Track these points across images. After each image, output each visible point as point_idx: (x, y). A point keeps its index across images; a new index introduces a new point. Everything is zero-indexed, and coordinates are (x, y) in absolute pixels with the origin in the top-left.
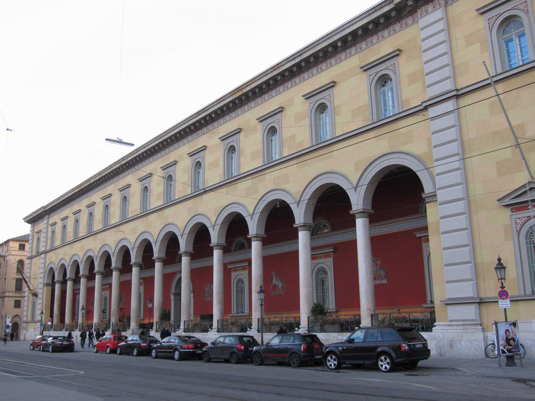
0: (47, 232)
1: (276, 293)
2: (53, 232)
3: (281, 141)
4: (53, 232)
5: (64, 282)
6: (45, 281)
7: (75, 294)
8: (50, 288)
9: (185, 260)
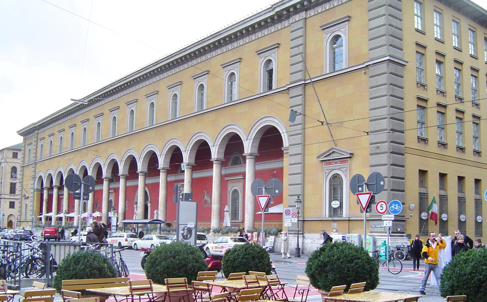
5: (51, 188)
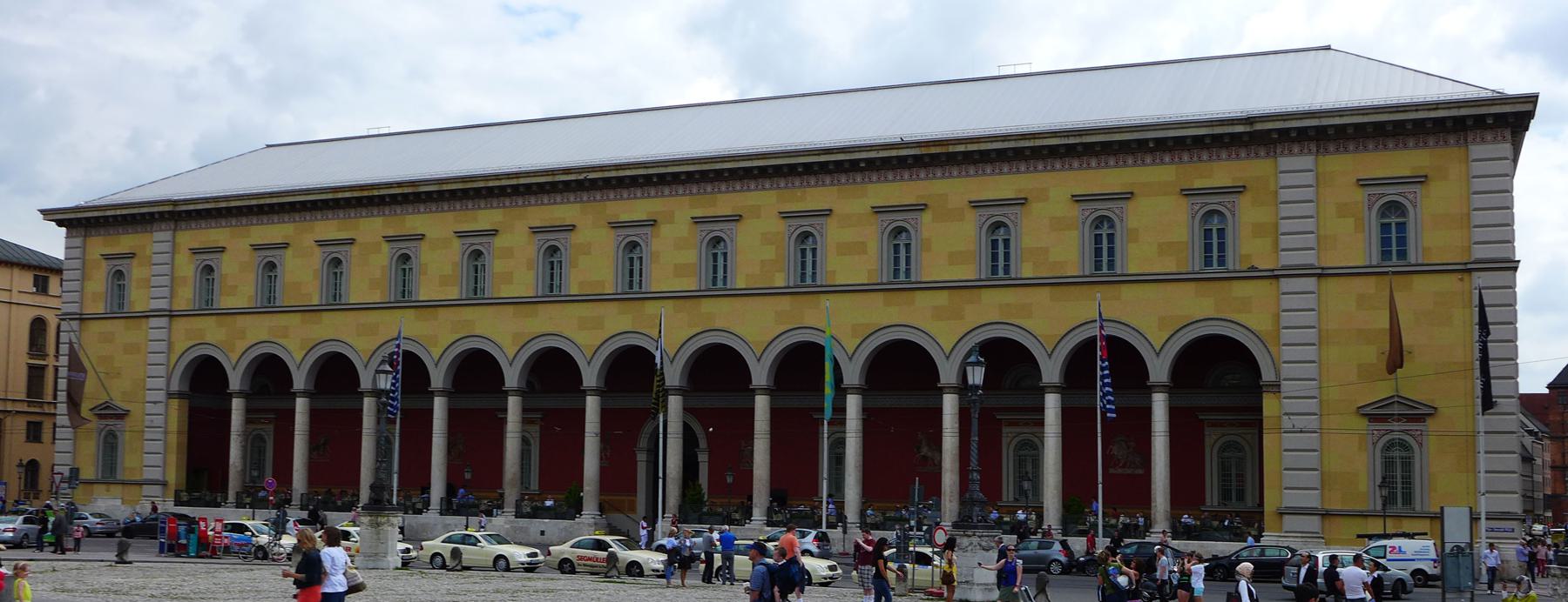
6: (175, 387)
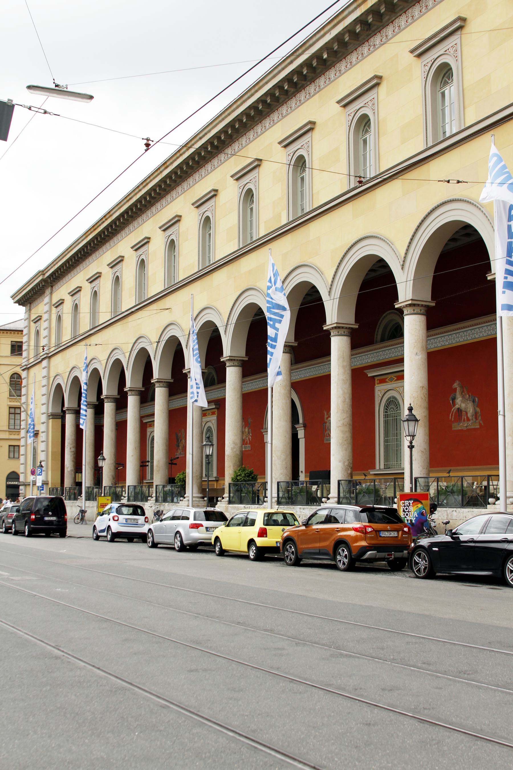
0: (50, 320)
1: (462, 426)
2: (59, 318)
3: (462, 93)
4: (59, 318)
6: (50, 411)
7: (145, 425)
8: (59, 421)
9: (413, 325)
